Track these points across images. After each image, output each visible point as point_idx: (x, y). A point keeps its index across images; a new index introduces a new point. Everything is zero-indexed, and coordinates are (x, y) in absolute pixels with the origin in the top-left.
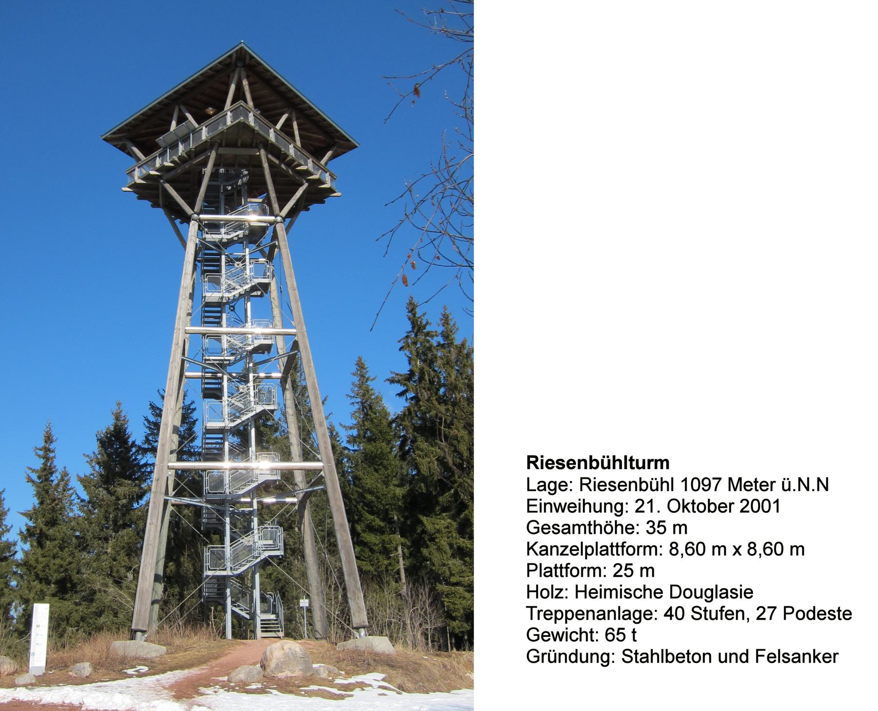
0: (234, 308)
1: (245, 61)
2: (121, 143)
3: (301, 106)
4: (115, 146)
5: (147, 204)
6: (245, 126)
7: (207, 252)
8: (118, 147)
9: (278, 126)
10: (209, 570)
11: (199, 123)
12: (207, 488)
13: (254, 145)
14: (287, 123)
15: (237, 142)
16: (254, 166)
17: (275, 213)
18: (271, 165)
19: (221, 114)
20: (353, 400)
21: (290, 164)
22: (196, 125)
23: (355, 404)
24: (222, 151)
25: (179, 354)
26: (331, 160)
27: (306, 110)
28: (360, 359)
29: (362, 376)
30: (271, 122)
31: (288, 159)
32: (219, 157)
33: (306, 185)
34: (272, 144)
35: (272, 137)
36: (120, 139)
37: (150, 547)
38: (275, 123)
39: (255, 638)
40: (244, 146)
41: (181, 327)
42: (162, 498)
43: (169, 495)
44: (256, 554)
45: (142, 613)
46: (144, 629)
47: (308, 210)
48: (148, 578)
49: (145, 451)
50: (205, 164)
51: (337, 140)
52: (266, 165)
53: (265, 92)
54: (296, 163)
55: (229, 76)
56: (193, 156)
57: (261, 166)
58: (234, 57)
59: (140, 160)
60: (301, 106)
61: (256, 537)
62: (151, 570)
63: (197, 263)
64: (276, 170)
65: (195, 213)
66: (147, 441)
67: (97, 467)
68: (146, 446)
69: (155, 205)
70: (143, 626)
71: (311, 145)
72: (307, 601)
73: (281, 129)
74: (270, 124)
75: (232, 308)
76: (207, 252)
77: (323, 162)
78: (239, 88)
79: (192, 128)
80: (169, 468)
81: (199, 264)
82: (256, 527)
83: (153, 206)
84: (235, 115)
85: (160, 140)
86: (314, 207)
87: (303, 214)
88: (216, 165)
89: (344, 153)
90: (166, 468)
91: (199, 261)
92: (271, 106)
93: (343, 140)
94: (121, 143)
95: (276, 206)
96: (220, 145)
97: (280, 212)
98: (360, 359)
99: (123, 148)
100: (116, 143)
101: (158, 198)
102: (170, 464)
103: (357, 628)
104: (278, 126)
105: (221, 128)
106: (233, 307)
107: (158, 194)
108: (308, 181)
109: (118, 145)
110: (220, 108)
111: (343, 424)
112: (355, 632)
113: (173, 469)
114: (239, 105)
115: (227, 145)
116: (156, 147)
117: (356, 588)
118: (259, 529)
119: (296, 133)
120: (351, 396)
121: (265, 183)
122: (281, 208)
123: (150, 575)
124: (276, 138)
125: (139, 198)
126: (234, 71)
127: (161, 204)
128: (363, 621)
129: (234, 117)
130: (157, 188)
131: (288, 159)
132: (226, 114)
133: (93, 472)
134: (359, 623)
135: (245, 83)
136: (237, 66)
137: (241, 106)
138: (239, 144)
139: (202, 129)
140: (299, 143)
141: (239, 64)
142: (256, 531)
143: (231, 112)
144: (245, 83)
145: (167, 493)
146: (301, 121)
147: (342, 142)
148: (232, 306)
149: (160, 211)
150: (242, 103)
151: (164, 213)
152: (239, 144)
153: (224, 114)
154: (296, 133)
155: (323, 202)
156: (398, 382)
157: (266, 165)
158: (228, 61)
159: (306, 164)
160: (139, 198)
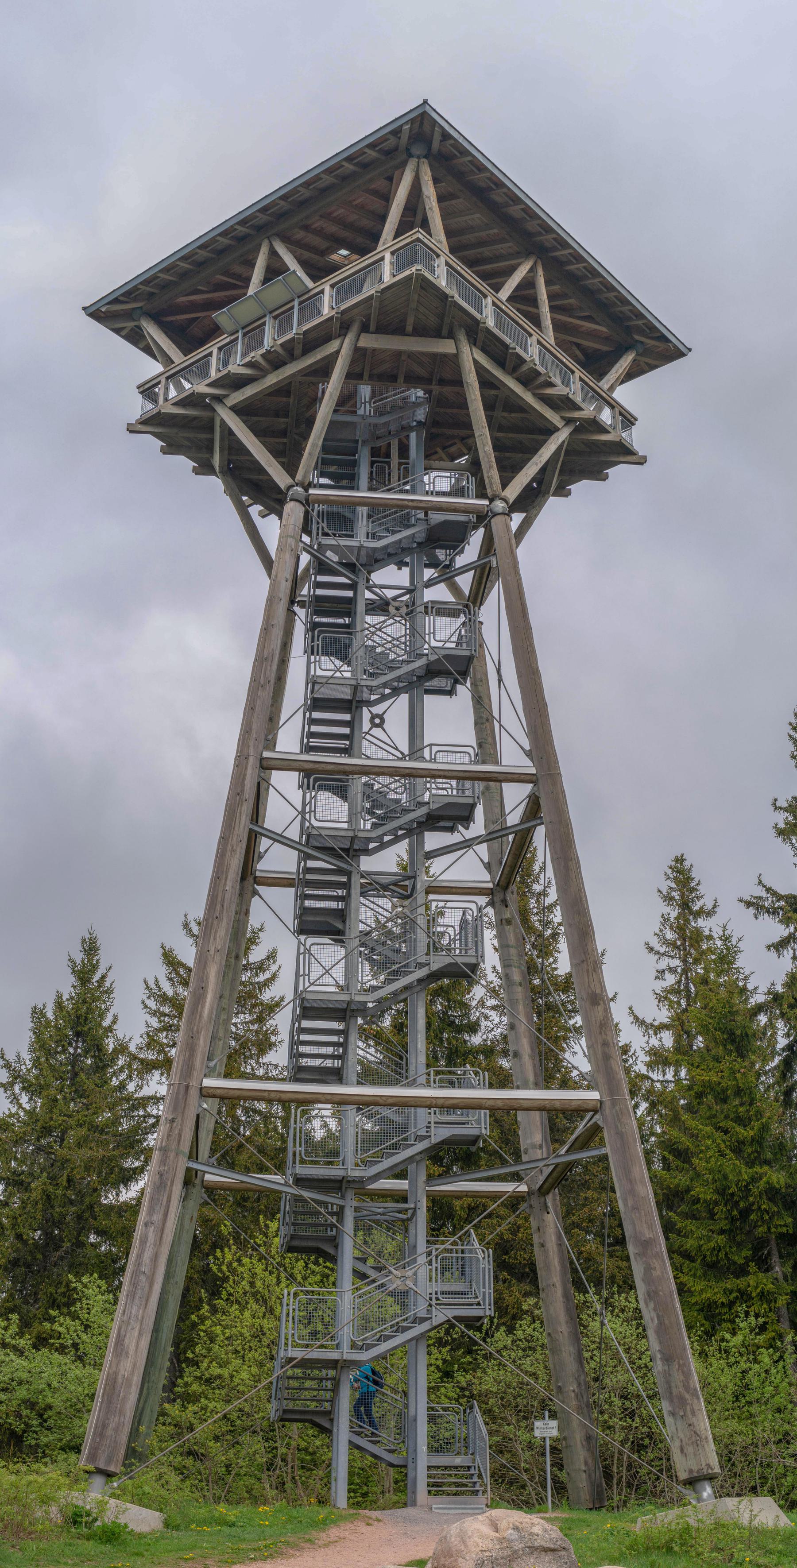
0: (383, 721)
1: (429, 143)
2: (130, 324)
4: (117, 331)
5: (183, 463)
6: (426, 286)
7: (320, 578)
8: (124, 333)
10: (302, 1161)
11: (314, 278)
12: (298, 1149)
13: (445, 332)
14: (527, 288)
15: (404, 321)
16: (442, 382)
17: (489, 492)
18: (487, 382)
20: (664, 963)
22: (310, 284)
23: (667, 975)
24: (368, 341)
25: (244, 818)
26: (622, 382)
27: (570, 263)
28: (680, 860)
29: (685, 905)
30: (484, 276)
31: (525, 368)
32: (359, 354)
33: (563, 435)
34: (488, 331)
35: (489, 318)
36: (129, 315)
37: (143, 1278)
38: (497, 288)
39: (414, 1504)
40: (420, 331)
41: (251, 752)
42: (183, 1163)
43: (200, 1160)
44: (421, 1309)
45: (109, 1432)
46: (112, 1468)
48: (131, 1353)
49: (148, 1067)
50: (324, 370)
51: (637, 337)
52: (471, 379)
53: (477, 218)
54: (542, 379)
55: (390, 179)
56: (298, 351)
57: (458, 382)
59: (173, 362)
61: (423, 1273)
62: (140, 1334)
63: (296, 608)
64: (493, 392)
65: (297, 485)
66: (151, 1042)
67: (24, 1099)
68: (151, 1056)
69: (204, 468)
70: (109, 1461)
71: (578, 346)
72: (554, 1424)
73: (510, 299)
74: (483, 286)
75: (377, 721)
76: (320, 578)
77: (605, 384)
79: (299, 289)
80: (205, 1093)
81: (301, 612)
82: (422, 1247)
83: (196, 471)
84: (402, 259)
85: (221, 317)
86: (581, 488)
87: (553, 503)
88: (353, 376)
89: (652, 367)
90: (194, 1093)
91: (302, 604)
92: (486, 251)
94: (130, 324)
95: (492, 474)
96: (365, 329)
98: (680, 860)
99: (136, 338)
101: (211, 450)
102: (208, 1082)
103: (692, 1482)
105: (369, 290)
106: (381, 717)
107: (212, 441)
108: (568, 421)
109: (123, 328)
111: (636, 1012)
112: (688, 1492)
113: (214, 1096)
114: (414, 237)
115: (382, 329)
117: (687, 1387)
118: (429, 1254)
120: (658, 953)
123: (137, 1346)
124: (499, 323)
126: (404, 164)
127: (217, 469)
128: (708, 1465)
129: (399, 266)
130: (209, 427)
132: (382, 259)
133: (14, 1110)
134: (695, 1468)
135: (429, 191)
136: (410, 156)
137: (418, 240)
138: (409, 328)
139: (322, 292)
140: (550, 337)
141: (417, 150)
142: (422, 1259)
143: (393, 253)
144: (429, 191)
145: (194, 1154)
146: (556, 288)
148: (377, 716)
149: (215, 484)
150: (420, 234)
151: (223, 487)
152: (409, 328)
156: (773, 912)
157: (471, 379)
158: (392, 141)
159: (566, 383)
160: (164, 451)
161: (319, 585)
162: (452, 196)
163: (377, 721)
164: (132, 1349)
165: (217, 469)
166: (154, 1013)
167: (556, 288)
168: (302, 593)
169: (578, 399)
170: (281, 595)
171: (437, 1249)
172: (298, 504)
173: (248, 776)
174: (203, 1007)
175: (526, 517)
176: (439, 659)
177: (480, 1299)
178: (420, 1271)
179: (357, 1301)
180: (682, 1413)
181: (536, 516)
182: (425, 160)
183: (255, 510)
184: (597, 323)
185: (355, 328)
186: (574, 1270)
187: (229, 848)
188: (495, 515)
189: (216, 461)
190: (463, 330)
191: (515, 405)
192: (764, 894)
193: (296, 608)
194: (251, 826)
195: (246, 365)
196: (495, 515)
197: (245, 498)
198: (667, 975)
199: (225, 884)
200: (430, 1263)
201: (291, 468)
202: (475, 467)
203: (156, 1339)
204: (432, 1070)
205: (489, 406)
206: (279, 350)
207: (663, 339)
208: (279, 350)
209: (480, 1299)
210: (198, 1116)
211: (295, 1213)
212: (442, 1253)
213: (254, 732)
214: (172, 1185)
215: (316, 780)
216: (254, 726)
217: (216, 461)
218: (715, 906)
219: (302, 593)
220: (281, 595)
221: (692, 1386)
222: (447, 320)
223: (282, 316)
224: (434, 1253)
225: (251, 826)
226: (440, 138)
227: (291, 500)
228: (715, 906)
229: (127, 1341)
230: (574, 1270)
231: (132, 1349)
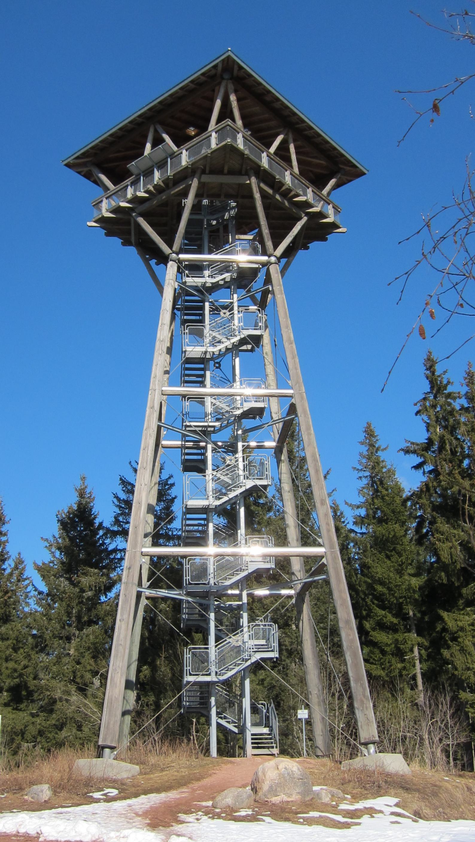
0: (220, 365)
2: (85, 169)
3: (300, 126)
4: (79, 173)
5: (116, 241)
8: (83, 174)
9: (272, 150)
10: (191, 675)
11: (178, 146)
12: (188, 578)
13: (243, 172)
16: (243, 197)
17: (268, 253)
18: (264, 195)
19: (204, 136)
20: (361, 474)
21: (287, 194)
22: (175, 148)
24: (206, 178)
25: (155, 419)
26: (334, 189)
28: (369, 425)
29: (372, 445)
30: (263, 144)
31: (284, 188)
32: (202, 186)
34: (265, 170)
35: (265, 162)
36: (84, 164)
38: (269, 146)
40: (231, 172)
42: (136, 589)
44: (245, 656)
47: (307, 248)
49: (114, 534)
50: (185, 194)
51: (341, 166)
52: (257, 196)
53: (257, 109)
55: (213, 91)
56: (171, 184)
57: (251, 197)
58: (220, 67)
59: (109, 190)
60: (300, 126)
61: (246, 636)
62: (121, 675)
63: (176, 311)
64: (269, 201)
68: (116, 528)
69: (127, 243)
71: (311, 171)
73: (276, 153)
74: (263, 147)
75: (217, 365)
77: (325, 192)
78: (226, 104)
80: (143, 554)
81: (178, 313)
83: (124, 244)
85: (133, 165)
86: (314, 246)
88: (199, 195)
89: (350, 181)
90: (139, 554)
91: (178, 309)
93: (349, 166)
94: (85, 169)
95: (269, 244)
96: (203, 172)
97: (275, 251)
99: (88, 176)
100: (79, 170)
101: (130, 234)
102: (144, 550)
104: (272, 150)
105: (204, 151)
106: (219, 363)
107: (130, 230)
110: (203, 128)
113: (148, 555)
114: (226, 124)
115: (212, 172)
116: (127, 174)
117: (364, 696)
118: (249, 627)
119: (294, 157)
120: (358, 470)
121: (256, 217)
122: (276, 247)
123: (120, 682)
125: (107, 235)
126: (219, 84)
127: (134, 244)
129: (220, 139)
130: (128, 223)
131: (284, 188)
132: (211, 135)
135: (233, 98)
136: (223, 79)
137: (228, 125)
138: (226, 171)
140: (296, 170)
141: (226, 76)
142: (246, 629)
144: (233, 98)
145: (140, 584)
146: (299, 143)
147: (348, 168)
148: (217, 363)
149: (132, 251)
150: (229, 122)
151: (136, 252)
152: (226, 171)
153: (210, 134)
154: (294, 157)
155: (325, 240)
157: (257, 196)
158: (213, 72)
160: (107, 235)
161: (187, 301)
162: (244, 98)
163: (217, 365)
164: (118, 682)
165: (134, 244)
166: (117, 506)
167: (299, 143)
168: (179, 304)
169: (311, 200)
170: (168, 309)
171: (252, 625)
172: (174, 262)
173: (156, 399)
174: (140, 513)
175: (287, 261)
176: (245, 338)
177: (273, 648)
178: (245, 635)
179: (217, 651)
180: (361, 708)
181: (292, 260)
182: (230, 81)
183: (153, 262)
184: (320, 160)
185: (199, 172)
186: (316, 632)
187: (148, 435)
188: (272, 264)
189: (133, 239)
190: (253, 171)
191: (279, 207)
192: (409, 445)
193: (176, 311)
194: (159, 423)
195: (145, 192)
196: (272, 264)
197: (147, 256)
198: (363, 479)
199: (147, 453)
200: (249, 632)
201: (170, 245)
202: (260, 238)
203: (129, 674)
204: (248, 537)
205: (266, 208)
206: (162, 184)
207: (355, 166)
208: (162, 184)
209: (273, 648)
210: (141, 565)
211: (189, 696)
212: (255, 626)
213: (158, 377)
214: (131, 600)
215: (188, 326)
216: (157, 375)
217: (133, 239)
218: (385, 449)
219: (179, 304)
220: (168, 309)
221: (366, 694)
222: (244, 166)
223: (162, 165)
224: (251, 627)
225: (159, 423)
226: (238, 69)
227: (171, 260)
228: (385, 449)
229: (115, 679)
230: (316, 632)
231: (118, 682)
